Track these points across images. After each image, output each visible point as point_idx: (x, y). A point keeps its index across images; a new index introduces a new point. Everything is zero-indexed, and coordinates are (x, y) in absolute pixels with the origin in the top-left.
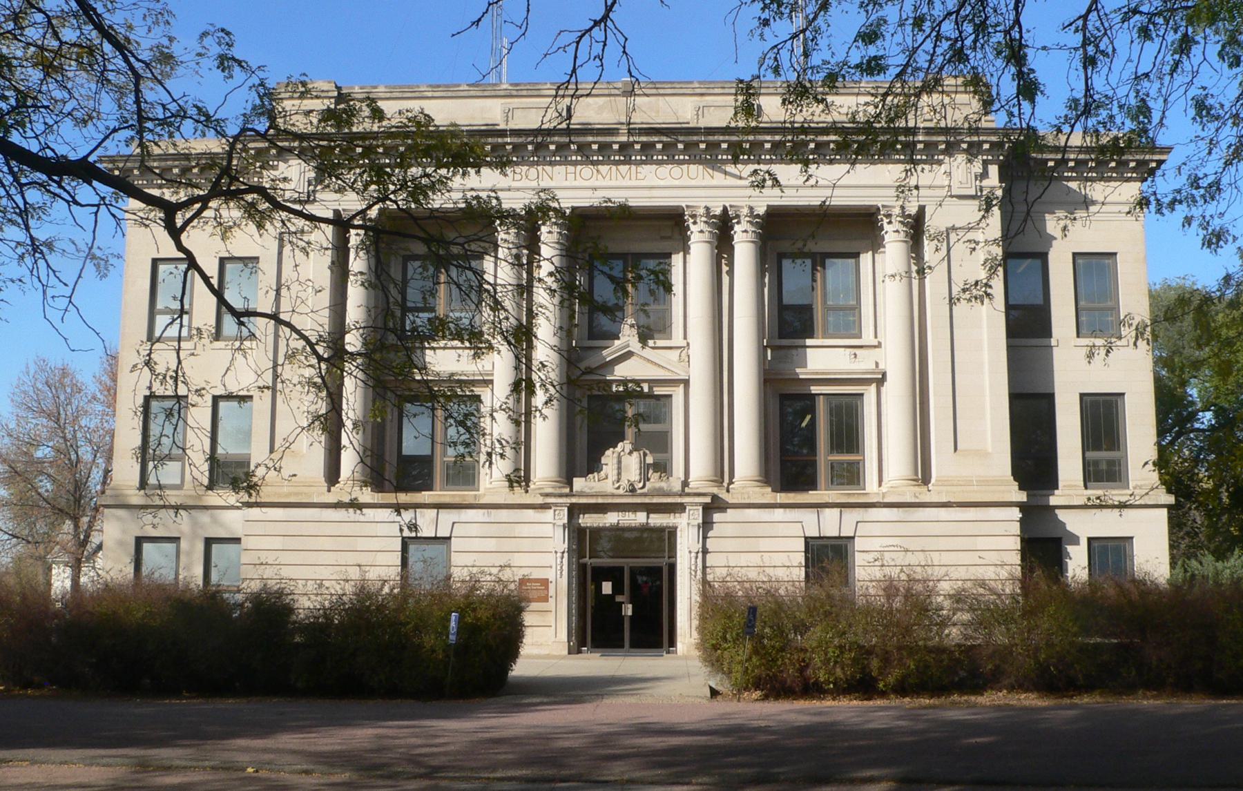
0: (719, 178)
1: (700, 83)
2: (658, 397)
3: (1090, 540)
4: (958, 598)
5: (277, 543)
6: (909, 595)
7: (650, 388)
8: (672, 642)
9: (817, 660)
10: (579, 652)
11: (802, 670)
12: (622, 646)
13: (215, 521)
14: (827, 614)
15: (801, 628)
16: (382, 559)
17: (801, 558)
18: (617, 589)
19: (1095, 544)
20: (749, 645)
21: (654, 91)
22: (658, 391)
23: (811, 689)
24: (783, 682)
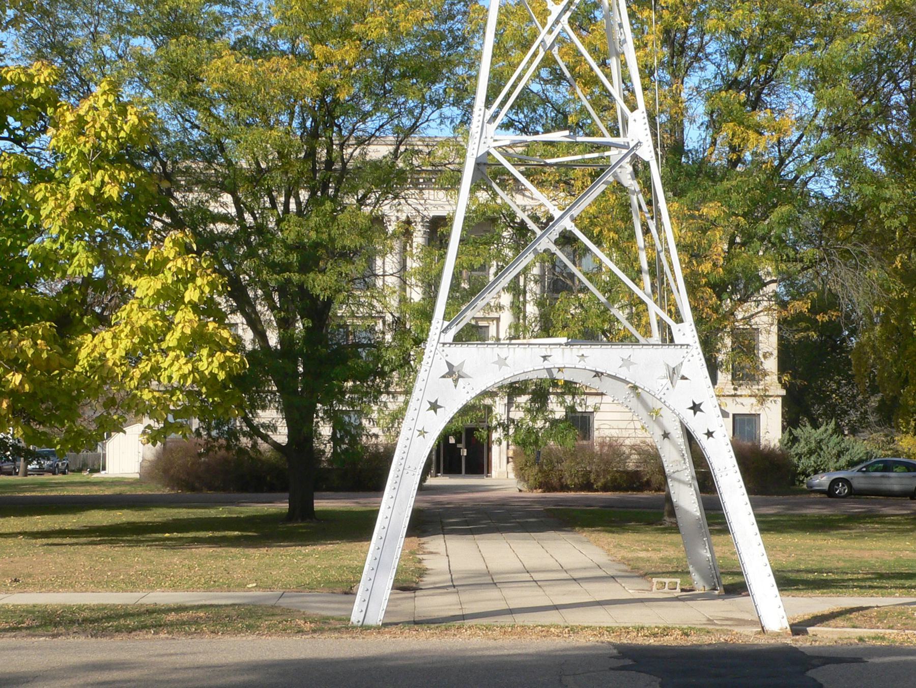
2: (481, 327)
3: (734, 415)
4: (632, 447)
6: (610, 446)
7: (477, 322)
8: (489, 471)
9: (567, 475)
10: (436, 476)
11: (560, 479)
12: (460, 472)
14: (572, 454)
15: (560, 461)
18: (458, 441)
19: (737, 418)
20: (537, 468)
22: (481, 324)
23: (564, 488)
24: (552, 484)
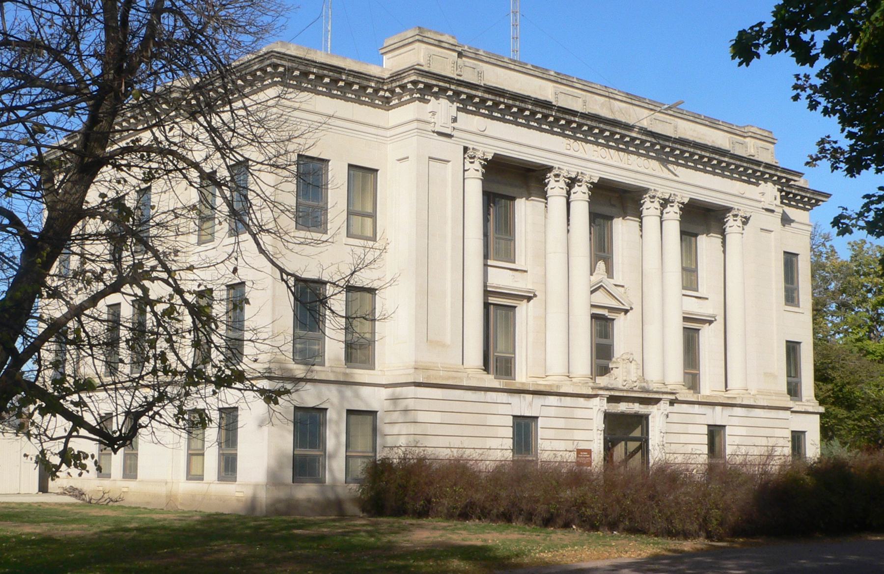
0: (665, 173)
1: (533, 66)
5: (437, 417)
13: (357, 395)
16: (781, 442)
17: (509, 432)
21: (629, 101)
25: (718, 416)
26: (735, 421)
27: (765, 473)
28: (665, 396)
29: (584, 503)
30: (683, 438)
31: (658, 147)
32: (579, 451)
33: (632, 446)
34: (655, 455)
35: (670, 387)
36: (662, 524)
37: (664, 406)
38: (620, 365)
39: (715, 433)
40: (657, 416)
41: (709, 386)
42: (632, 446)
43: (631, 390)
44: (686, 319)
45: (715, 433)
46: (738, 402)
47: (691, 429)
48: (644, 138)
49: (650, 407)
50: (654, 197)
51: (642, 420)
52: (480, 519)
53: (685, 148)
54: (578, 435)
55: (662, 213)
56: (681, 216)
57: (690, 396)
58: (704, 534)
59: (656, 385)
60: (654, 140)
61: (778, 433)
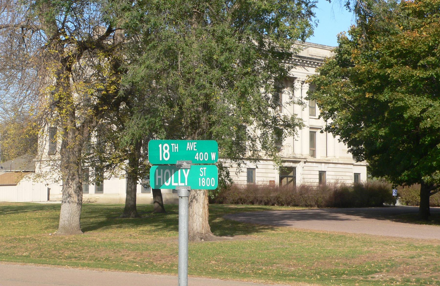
25: (323, 167)
26: (330, 169)
27: (335, 187)
28: (302, 160)
29: (279, 197)
30: (309, 176)
31: (301, 61)
32: (270, 181)
33: (290, 179)
34: (299, 182)
35: (304, 156)
36: (304, 203)
37: (302, 164)
38: (285, 148)
39: (322, 174)
40: (299, 168)
41: (320, 156)
42: (290, 179)
43: (289, 158)
44: (311, 128)
45: (322, 174)
46: (331, 162)
47: (312, 172)
48: (296, 58)
49: (297, 164)
50: (299, 81)
51: (293, 169)
52: (242, 204)
53: (311, 61)
54: (270, 175)
55: (302, 86)
56: (309, 87)
57: (312, 159)
58: (316, 206)
59: (299, 156)
60: (299, 59)
61: (347, 174)
